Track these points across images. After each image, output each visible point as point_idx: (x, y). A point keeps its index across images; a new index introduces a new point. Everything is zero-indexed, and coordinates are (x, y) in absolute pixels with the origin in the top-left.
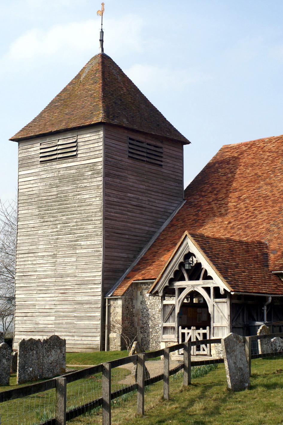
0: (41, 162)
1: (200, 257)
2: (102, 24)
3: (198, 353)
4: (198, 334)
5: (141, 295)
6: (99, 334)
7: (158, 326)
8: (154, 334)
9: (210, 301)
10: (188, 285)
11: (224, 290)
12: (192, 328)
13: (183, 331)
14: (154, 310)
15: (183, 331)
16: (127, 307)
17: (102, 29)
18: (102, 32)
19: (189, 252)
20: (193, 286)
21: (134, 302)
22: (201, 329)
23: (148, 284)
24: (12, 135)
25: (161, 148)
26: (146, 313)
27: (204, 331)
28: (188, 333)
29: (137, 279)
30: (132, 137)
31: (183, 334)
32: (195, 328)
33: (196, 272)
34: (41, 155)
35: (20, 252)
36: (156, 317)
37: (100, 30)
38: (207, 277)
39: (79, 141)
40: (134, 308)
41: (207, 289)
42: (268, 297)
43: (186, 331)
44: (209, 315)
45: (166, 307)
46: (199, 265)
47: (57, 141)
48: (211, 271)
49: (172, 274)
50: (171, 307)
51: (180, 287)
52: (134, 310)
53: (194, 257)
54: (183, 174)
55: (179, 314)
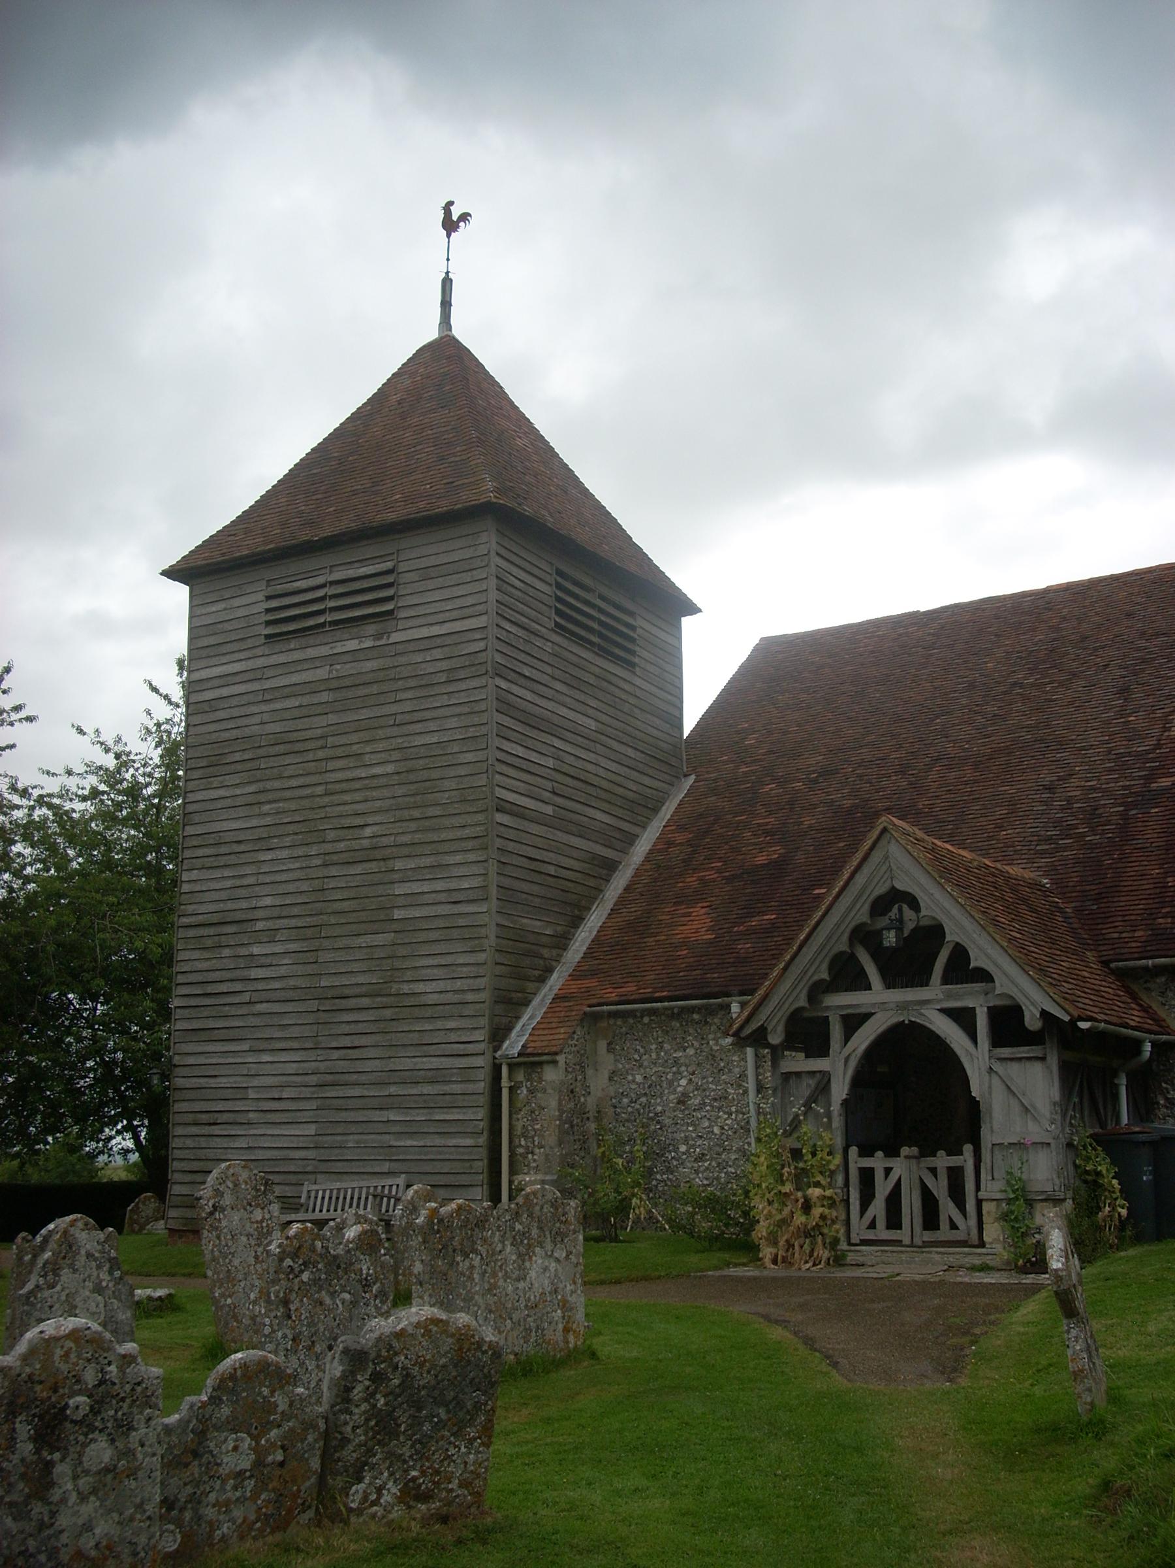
0: (267, 636)
1: (940, 904)
2: (448, 260)
3: (928, 1236)
4: (927, 1171)
5: (608, 1051)
6: (483, 1178)
7: (676, 1150)
8: (659, 1177)
9: (975, 1057)
10: (883, 1004)
11: (1044, 1013)
12: (905, 1151)
13: (867, 1162)
14: (659, 1100)
15: (867, 1162)
16: (572, 1092)
17: (447, 273)
18: (447, 283)
19: (893, 887)
20: (903, 1006)
21: (590, 1072)
22: (941, 1153)
23: (635, 1016)
24: (175, 555)
25: (632, 614)
26: (630, 1109)
27: (954, 1161)
28: (888, 1171)
29: (602, 1000)
30: (564, 568)
31: (867, 1176)
32: (915, 1150)
33: (916, 954)
34: (270, 617)
35: (185, 921)
36: (667, 1121)
37: (444, 275)
38: (961, 969)
39: (403, 567)
40: (589, 1093)
41: (963, 1018)
42: (1138, 1043)
43: (877, 1162)
44: (974, 1105)
45: (793, 1081)
46: (935, 932)
47: (328, 571)
48: (984, 951)
49: (825, 966)
50: (812, 1082)
51: (849, 1011)
52: (589, 1099)
53: (905, 907)
54: (682, 702)
55: (845, 1103)
